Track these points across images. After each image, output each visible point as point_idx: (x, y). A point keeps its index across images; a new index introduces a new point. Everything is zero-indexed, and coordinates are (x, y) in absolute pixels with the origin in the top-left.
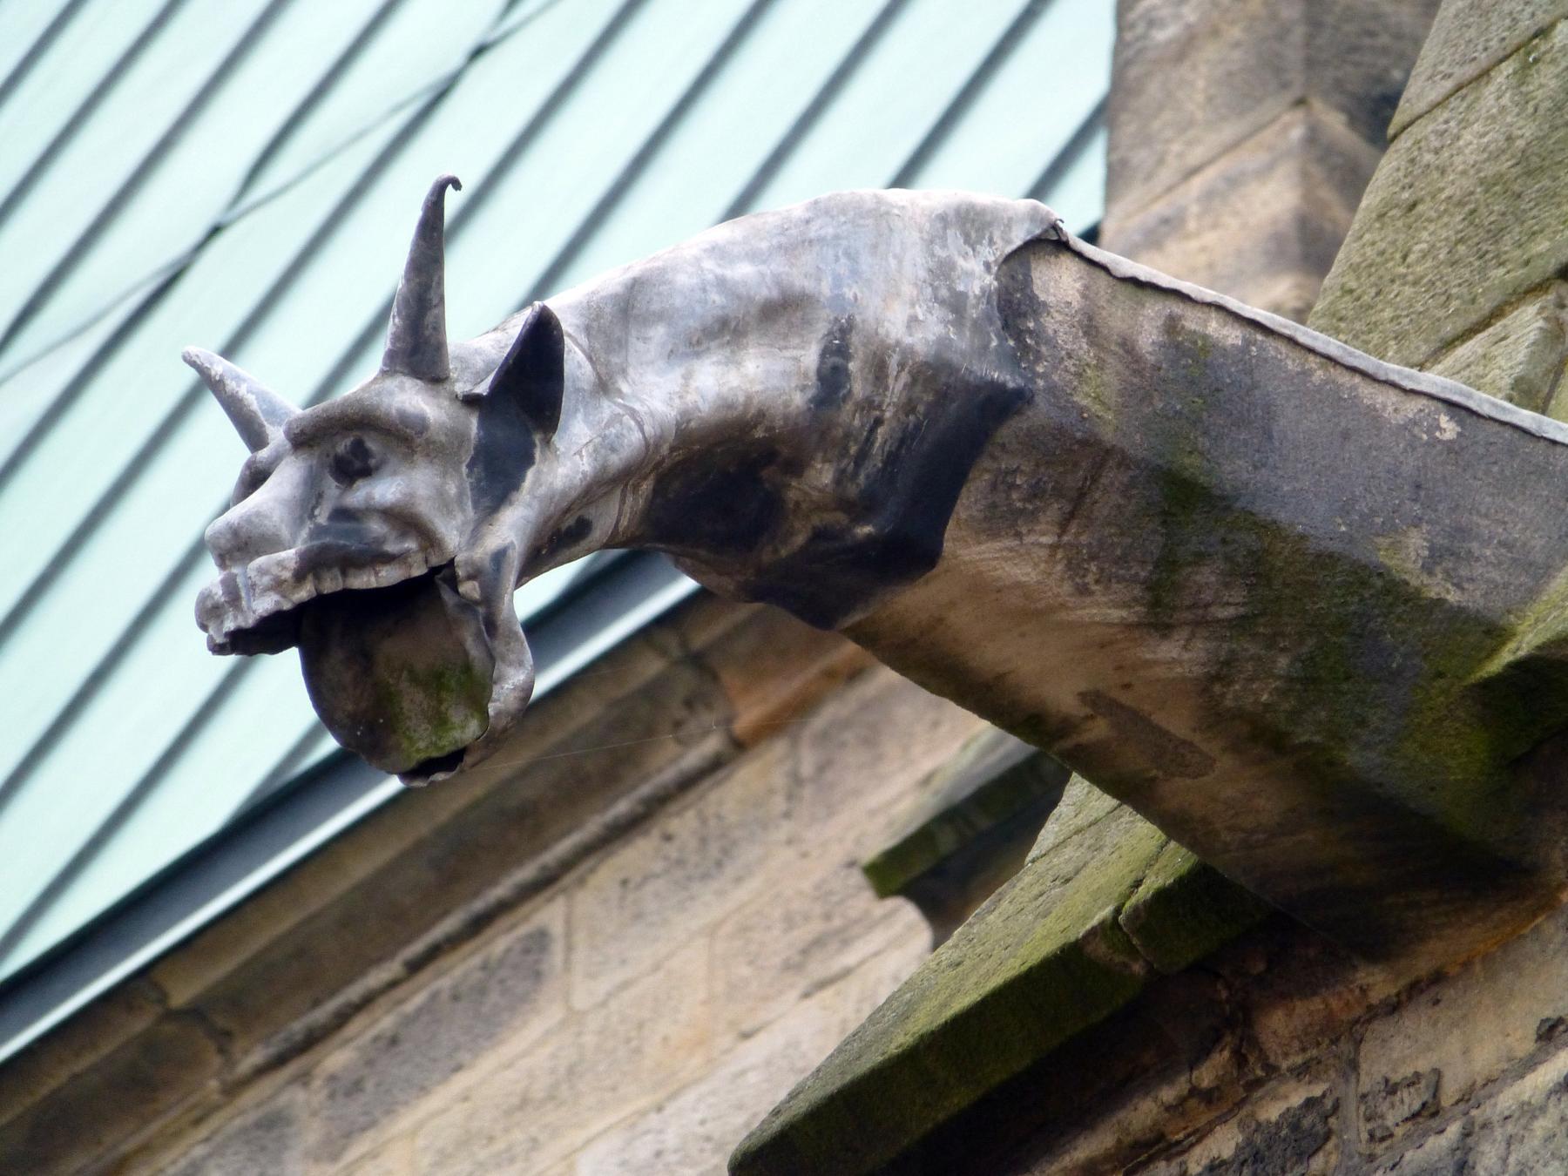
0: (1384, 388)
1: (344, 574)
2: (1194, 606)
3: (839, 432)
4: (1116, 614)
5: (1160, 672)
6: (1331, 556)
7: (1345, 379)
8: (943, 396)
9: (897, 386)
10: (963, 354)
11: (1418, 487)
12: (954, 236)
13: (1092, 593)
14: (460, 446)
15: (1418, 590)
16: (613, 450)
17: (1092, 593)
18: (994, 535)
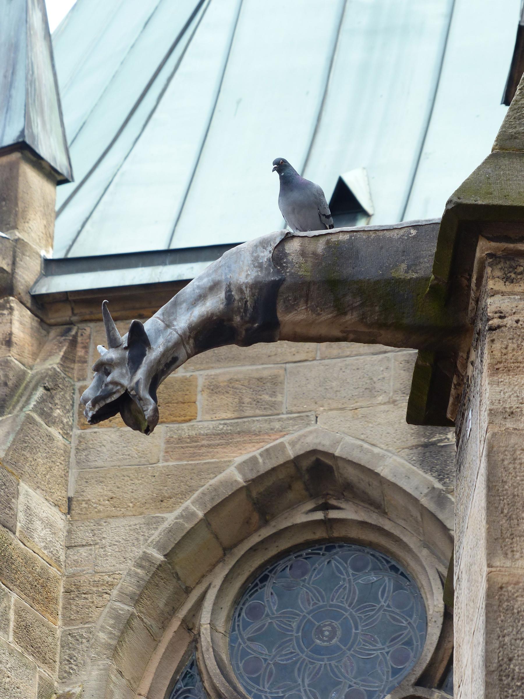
0: (393, 231)
1: (105, 401)
2: (349, 306)
3: (236, 309)
4: (330, 316)
5: (349, 322)
6: (378, 281)
7: (381, 233)
8: (261, 289)
9: (247, 292)
10: (263, 277)
11: (404, 252)
12: (260, 249)
13: (321, 314)
14: (124, 360)
15: (404, 279)
16: (169, 342)
17: (321, 314)
18: (290, 312)
